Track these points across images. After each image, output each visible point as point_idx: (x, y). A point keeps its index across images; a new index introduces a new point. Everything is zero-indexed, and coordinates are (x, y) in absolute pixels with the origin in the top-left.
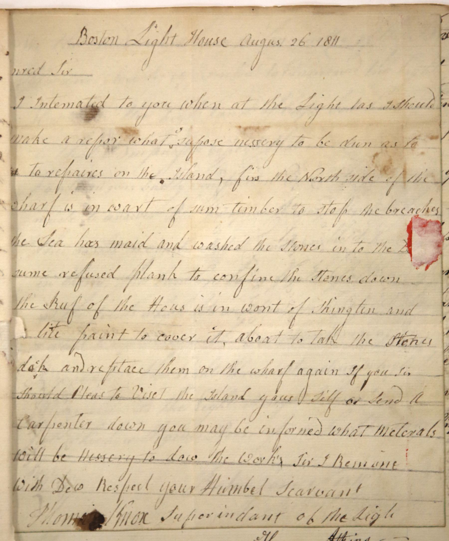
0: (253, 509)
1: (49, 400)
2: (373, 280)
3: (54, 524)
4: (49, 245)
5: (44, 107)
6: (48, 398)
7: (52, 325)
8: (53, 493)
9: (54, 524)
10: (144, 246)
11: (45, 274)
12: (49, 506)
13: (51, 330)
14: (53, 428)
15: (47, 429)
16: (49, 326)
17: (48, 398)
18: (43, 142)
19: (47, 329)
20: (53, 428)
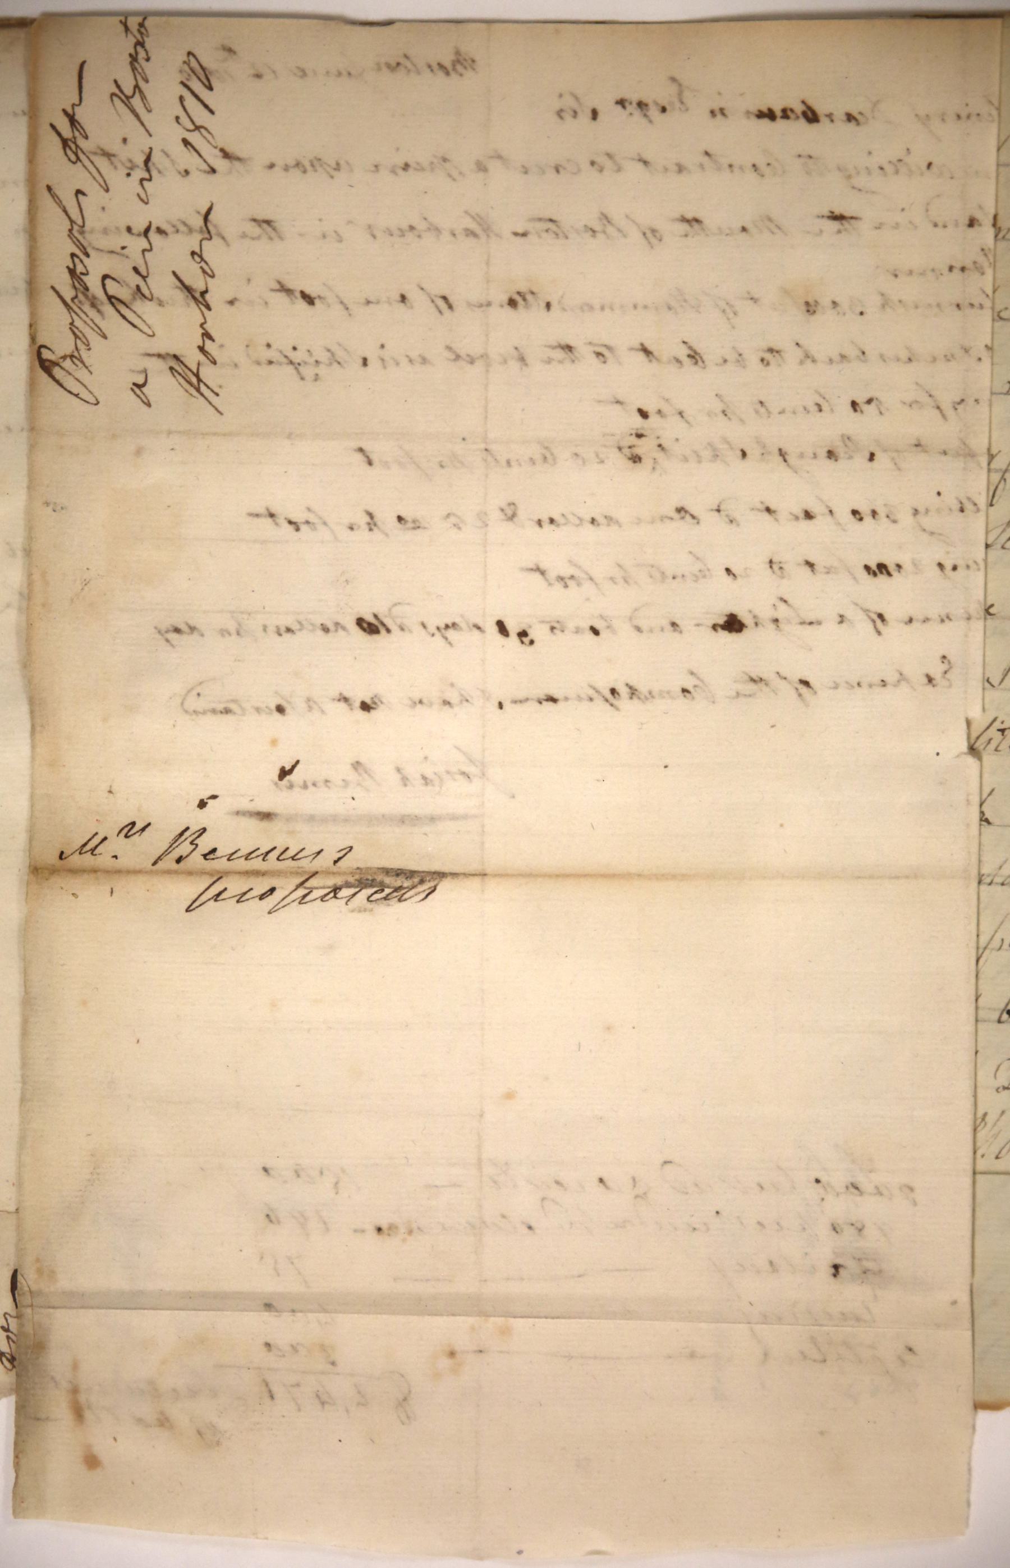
0: (785, 598)
1: (992, 887)
2: (753, 359)
3: (997, 1158)
4: (1003, 547)
5: (1004, 237)
6: (990, 884)
7: (1002, 723)
8: (997, 1090)
9: (997, 1158)
10: (142, 180)
11: (991, 611)
12: (987, 1119)
13: (1000, 733)
14: (1000, 949)
15: (987, 952)
16: (997, 725)
17: (990, 884)
18: (998, 316)
19: (993, 732)
20: (1000, 949)
